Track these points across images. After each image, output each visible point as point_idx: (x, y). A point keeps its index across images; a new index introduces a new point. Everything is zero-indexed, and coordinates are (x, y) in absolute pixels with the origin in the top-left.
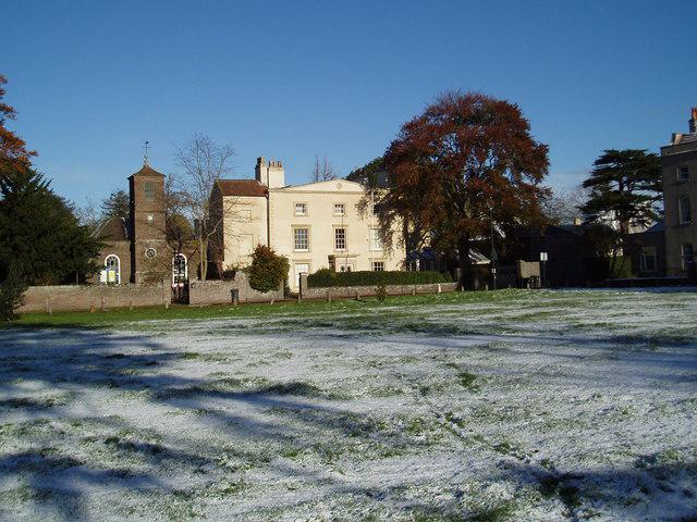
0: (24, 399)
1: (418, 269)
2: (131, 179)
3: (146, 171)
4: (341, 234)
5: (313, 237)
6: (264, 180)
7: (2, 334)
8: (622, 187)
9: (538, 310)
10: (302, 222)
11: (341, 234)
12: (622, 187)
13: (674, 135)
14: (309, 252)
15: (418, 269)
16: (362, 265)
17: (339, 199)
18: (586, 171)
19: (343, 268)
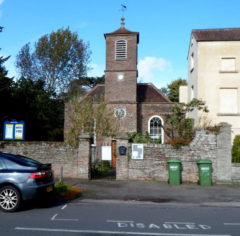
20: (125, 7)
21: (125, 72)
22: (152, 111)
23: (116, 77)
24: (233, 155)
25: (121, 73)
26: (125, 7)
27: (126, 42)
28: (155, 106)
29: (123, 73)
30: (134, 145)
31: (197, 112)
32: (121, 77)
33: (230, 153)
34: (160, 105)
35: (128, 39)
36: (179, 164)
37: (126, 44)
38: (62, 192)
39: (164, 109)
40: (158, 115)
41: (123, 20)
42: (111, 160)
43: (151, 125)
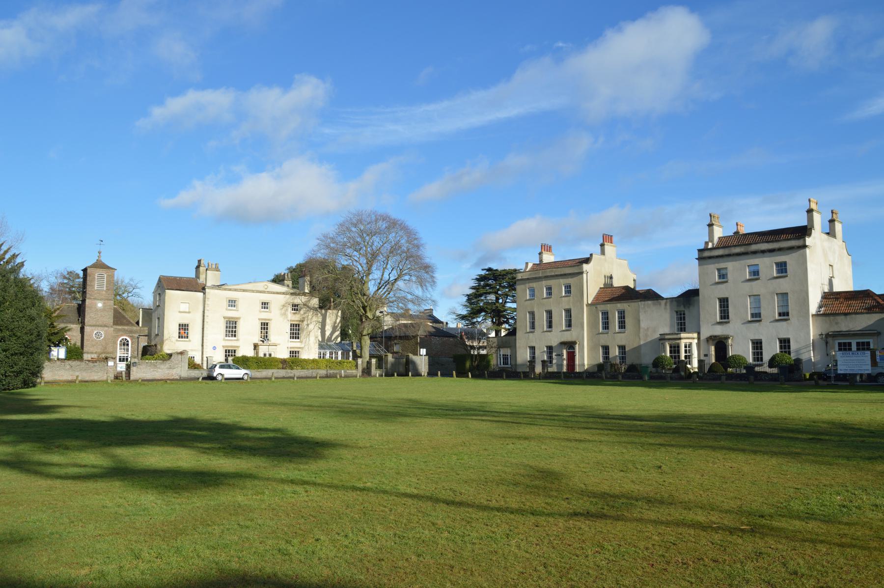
0: (66, 473)
1: (340, 358)
2: (85, 270)
3: (99, 265)
4: (265, 326)
5: (241, 328)
6: (202, 280)
7: (882, 441)
8: (497, 299)
9: (820, 437)
10: (232, 314)
11: (265, 326)
12: (497, 299)
13: (527, 264)
14: (237, 340)
15: (340, 358)
16: (282, 353)
17: (265, 297)
18: (466, 286)
19: (265, 355)
20: (102, 241)
22: (121, 333)
23: (96, 304)
24: (189, 365)
25: (101, 301)
26: (102, 241)
27: (105, 276)
28: (124, 329)
29: (102, 302)
31: (699, 285)
32: (100, 305)
33: (187, 364)
34: (671, 534)
35: (108, 274)
36: (208, 271)
37: (105, 278)
38: (68, 368)
39: (131, 332)
40: (126, 336)
41: (99, 253)
42: (544, 262)
43: (120, 345)
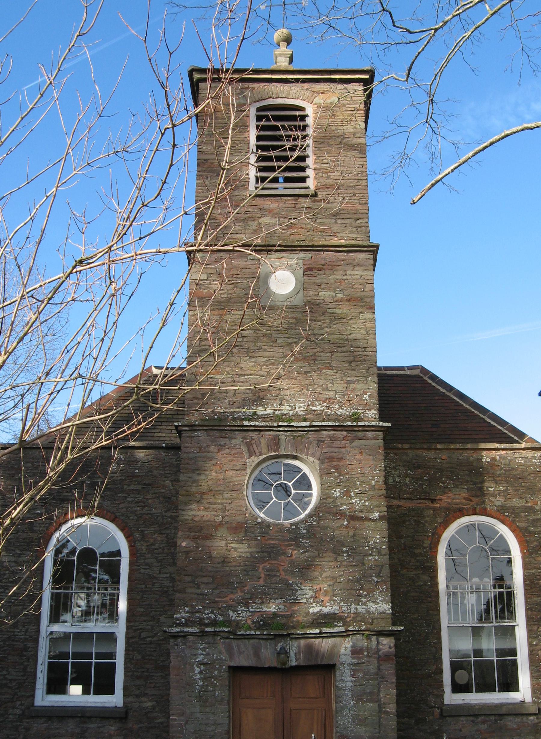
21: (308, 255)
30: (110, 691)
